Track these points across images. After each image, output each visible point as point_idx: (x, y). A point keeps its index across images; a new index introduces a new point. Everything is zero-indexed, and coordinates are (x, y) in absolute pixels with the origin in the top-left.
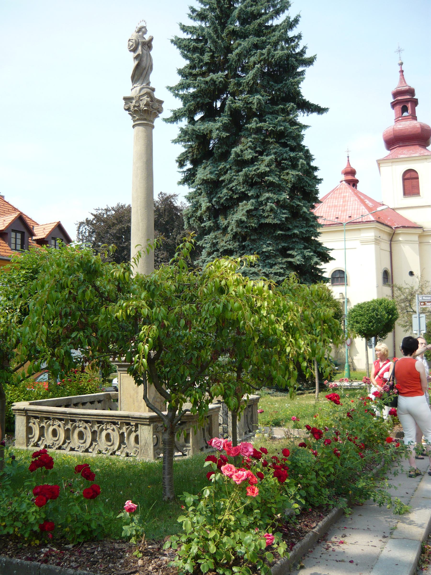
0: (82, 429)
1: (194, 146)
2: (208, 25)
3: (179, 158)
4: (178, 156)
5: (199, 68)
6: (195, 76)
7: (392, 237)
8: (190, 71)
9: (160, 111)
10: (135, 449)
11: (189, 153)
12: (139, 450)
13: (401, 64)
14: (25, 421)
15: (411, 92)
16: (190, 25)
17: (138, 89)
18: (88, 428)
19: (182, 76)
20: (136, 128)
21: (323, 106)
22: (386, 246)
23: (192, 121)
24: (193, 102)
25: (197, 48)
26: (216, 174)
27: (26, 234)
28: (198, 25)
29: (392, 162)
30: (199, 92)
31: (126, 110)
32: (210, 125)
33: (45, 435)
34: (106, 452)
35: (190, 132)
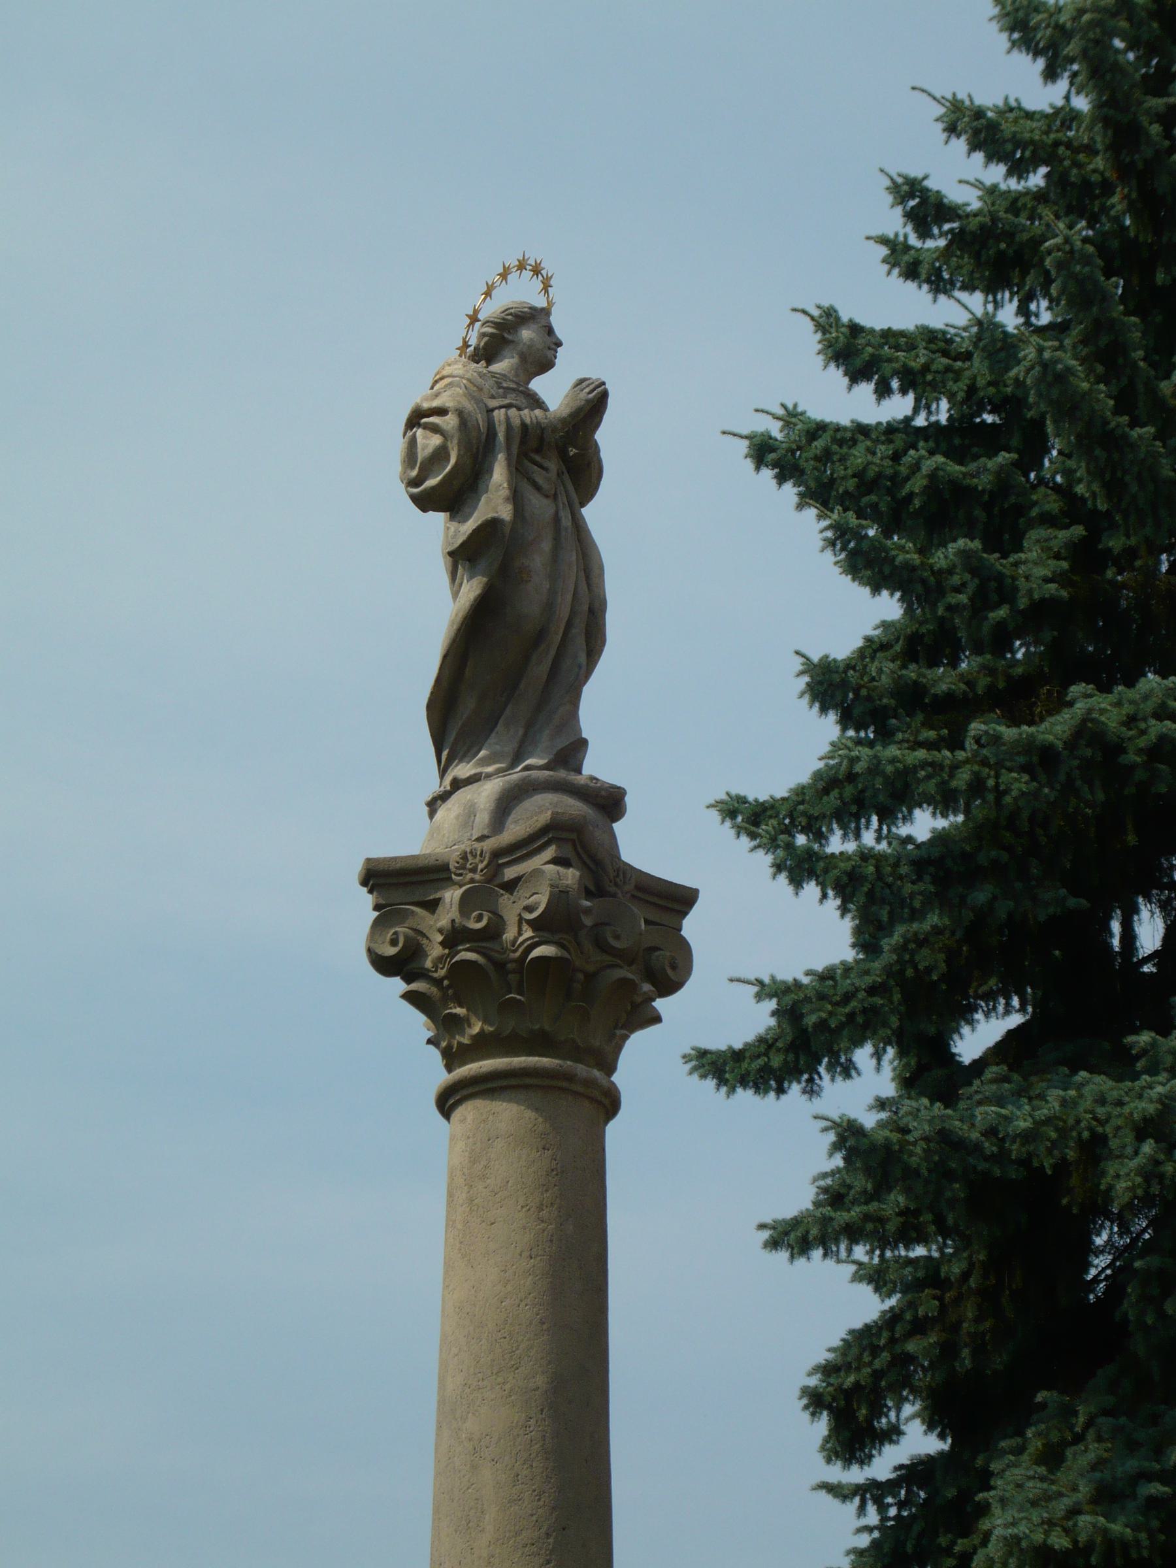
1: (956, 1269)
2: (1045, 318)
3: (827, 1370)
4: (822, 1356)
5: (978, 650)
6: (951, 713)
8: (912, 672)
9: (668, 969)
11: (919, 1327)
16: (905, 321)
17: (485, 794)
19: (845, 721)
20: (468, 1112)
23: (930, 1070)
24: (934, 919)
25: (960, 492)
26: (1153, 1503)
28: (961, 319)
30: (979, 832)
31: (384, 965)
32: (1084, 1094)
35: (916, 1157)
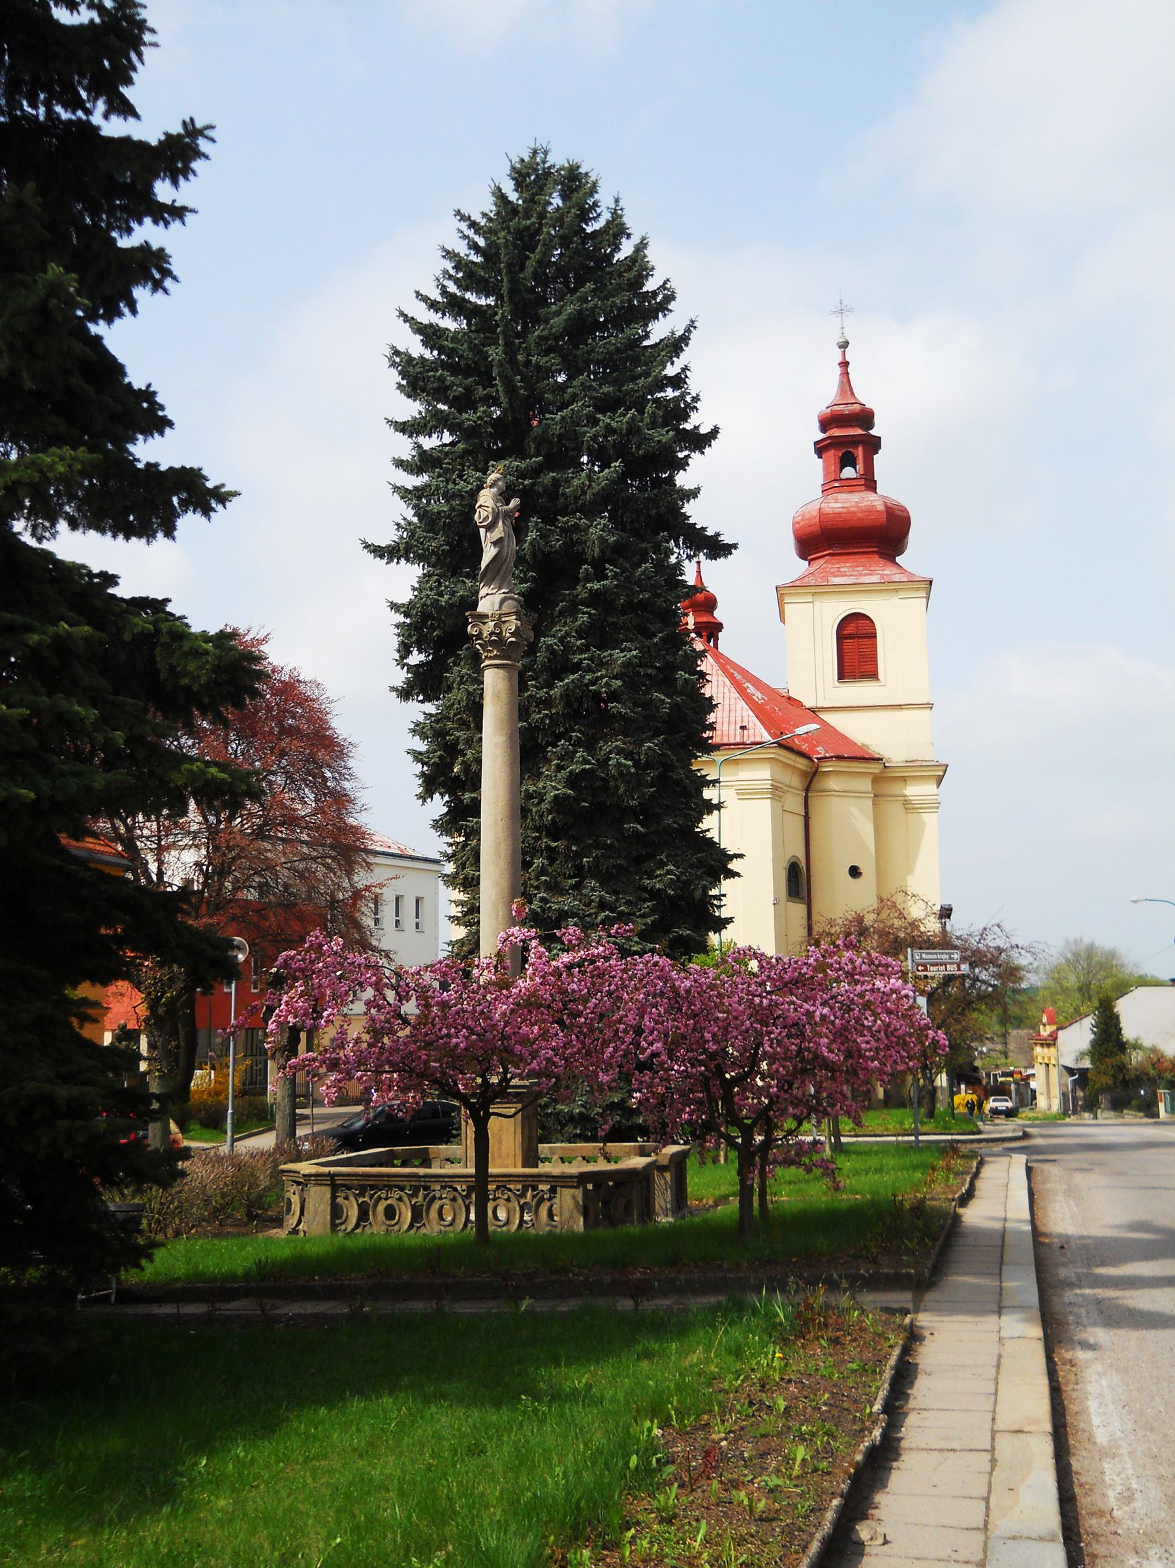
7: (811, 780)
13: (844, 345)
14: (329, 1195)
15: (865, 418)
18: (406, 1199)
21: (726, 539)
22: (795, 803)
29: (814, 594)
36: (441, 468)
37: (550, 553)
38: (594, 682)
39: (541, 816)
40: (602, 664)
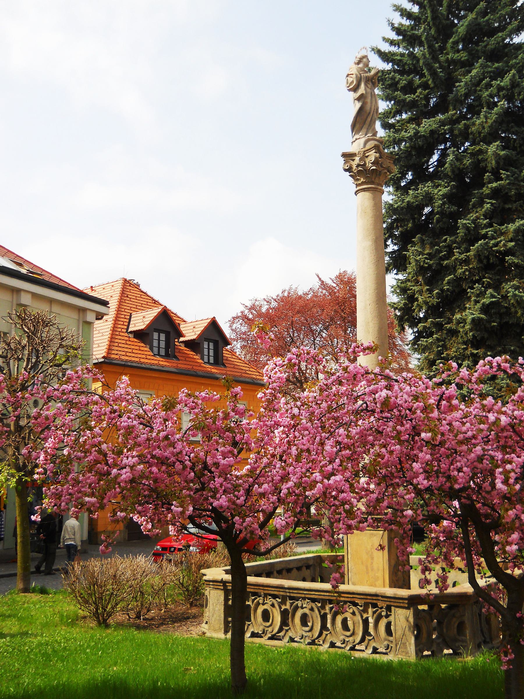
0: (306, 611)
10: (386, 643)
12: (393, 645)
14: (222, 598)
17: (362, 141)
18: (276, 605)
20: (360, 195)
27: (172, 334)
31: (346, 170)
33: (290, 624)
34: (343, 646)
36: (394, 129)
37: (463, 169)
38: (496, 245)
39: (466, 334)
40: (502, 234)
